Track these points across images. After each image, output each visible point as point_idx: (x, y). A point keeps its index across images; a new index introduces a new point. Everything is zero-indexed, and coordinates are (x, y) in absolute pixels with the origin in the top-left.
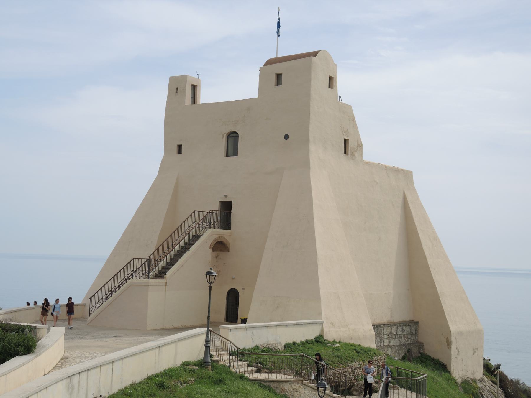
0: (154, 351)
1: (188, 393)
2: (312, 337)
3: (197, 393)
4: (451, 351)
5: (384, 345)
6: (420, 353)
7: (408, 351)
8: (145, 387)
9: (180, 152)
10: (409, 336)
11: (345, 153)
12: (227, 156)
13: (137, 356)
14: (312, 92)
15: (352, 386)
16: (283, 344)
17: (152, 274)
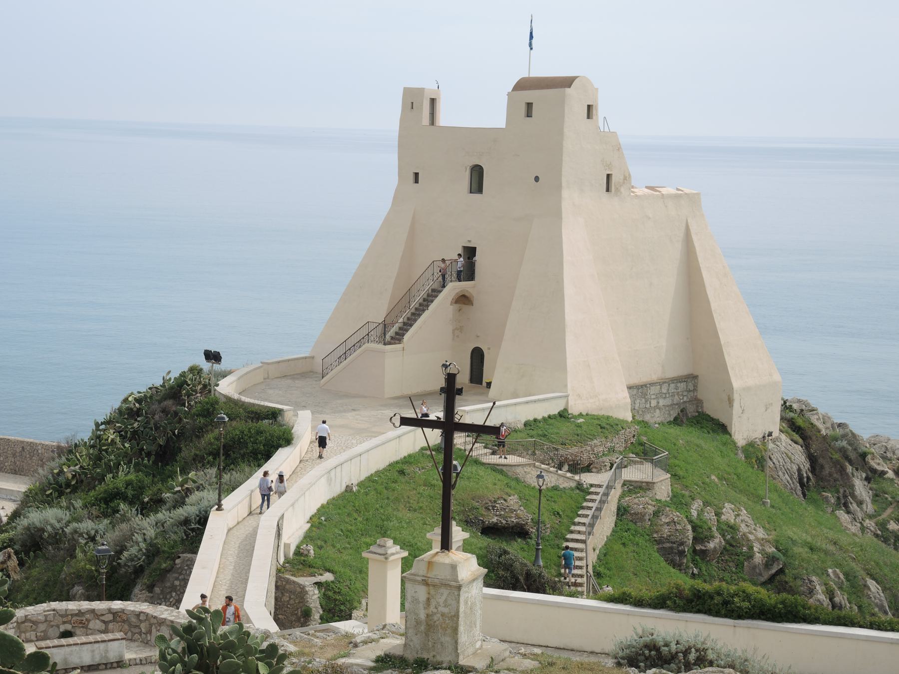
0: (395, 441)
1: (425, 479)
2: (555, 412)
3: (434, 479)
4: (732, 410)
5: (650, 406)
6: (697, 412)
7: (682, 411)
8: (388, 474)
9: (417, 181)
10: (685, 393)
11: (608, 190)
12: (471, 192)
13: (380, 447)
14: (566, 130)
15: (592, 464)
16: (523, 422)
17: (388, 338)
